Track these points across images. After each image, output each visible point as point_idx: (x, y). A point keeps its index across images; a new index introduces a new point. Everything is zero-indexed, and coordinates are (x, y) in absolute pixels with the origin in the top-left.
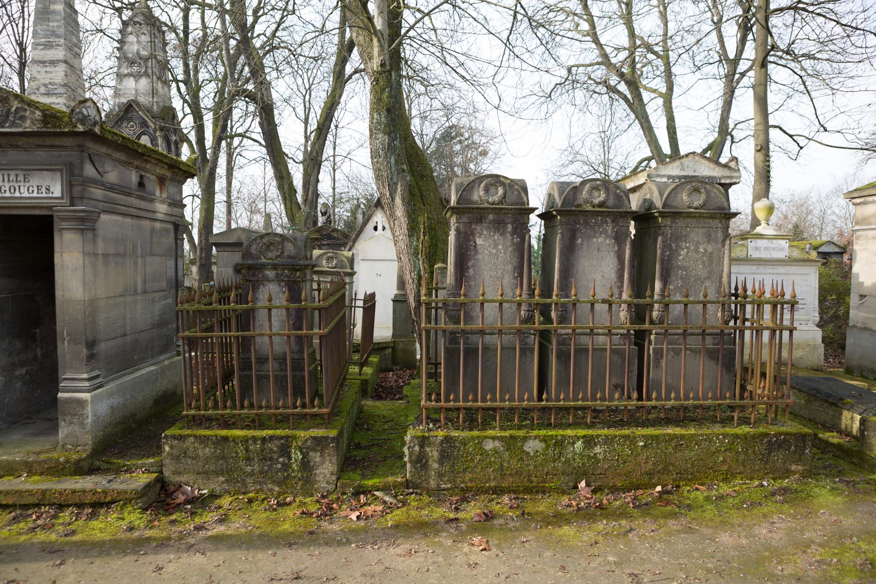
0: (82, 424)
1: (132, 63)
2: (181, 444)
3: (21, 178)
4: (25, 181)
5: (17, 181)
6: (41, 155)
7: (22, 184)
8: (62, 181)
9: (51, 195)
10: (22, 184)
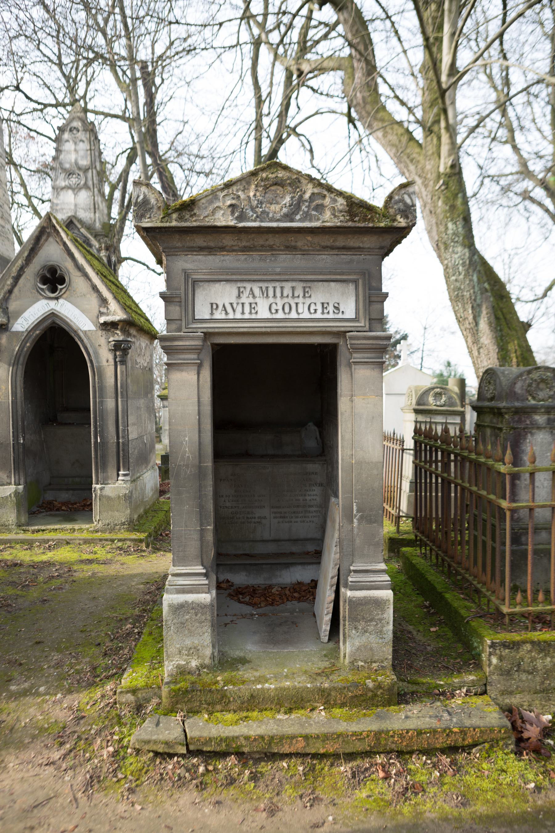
0: (380, 633)
1: (70, 174)
2: (514, 654)
3: (299, 292)
4: (304, 296)
5: (293, 297)
6: (325, 260)
7: (301, 300)
8: (357, 296)
9: (340, 316)
10: (301, 300)
